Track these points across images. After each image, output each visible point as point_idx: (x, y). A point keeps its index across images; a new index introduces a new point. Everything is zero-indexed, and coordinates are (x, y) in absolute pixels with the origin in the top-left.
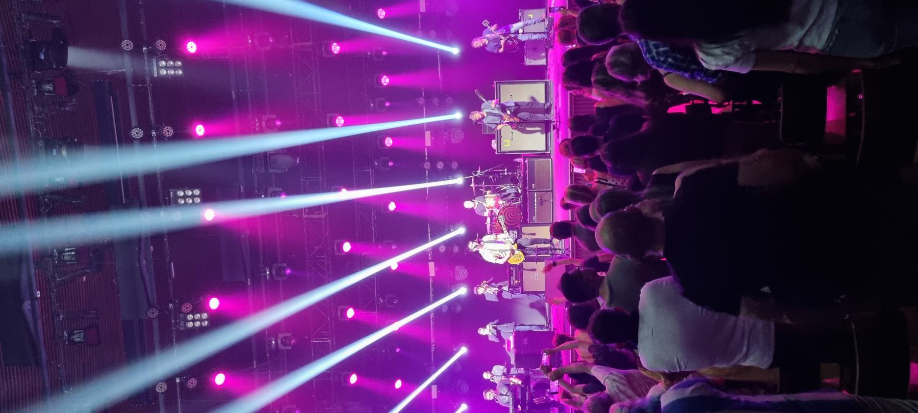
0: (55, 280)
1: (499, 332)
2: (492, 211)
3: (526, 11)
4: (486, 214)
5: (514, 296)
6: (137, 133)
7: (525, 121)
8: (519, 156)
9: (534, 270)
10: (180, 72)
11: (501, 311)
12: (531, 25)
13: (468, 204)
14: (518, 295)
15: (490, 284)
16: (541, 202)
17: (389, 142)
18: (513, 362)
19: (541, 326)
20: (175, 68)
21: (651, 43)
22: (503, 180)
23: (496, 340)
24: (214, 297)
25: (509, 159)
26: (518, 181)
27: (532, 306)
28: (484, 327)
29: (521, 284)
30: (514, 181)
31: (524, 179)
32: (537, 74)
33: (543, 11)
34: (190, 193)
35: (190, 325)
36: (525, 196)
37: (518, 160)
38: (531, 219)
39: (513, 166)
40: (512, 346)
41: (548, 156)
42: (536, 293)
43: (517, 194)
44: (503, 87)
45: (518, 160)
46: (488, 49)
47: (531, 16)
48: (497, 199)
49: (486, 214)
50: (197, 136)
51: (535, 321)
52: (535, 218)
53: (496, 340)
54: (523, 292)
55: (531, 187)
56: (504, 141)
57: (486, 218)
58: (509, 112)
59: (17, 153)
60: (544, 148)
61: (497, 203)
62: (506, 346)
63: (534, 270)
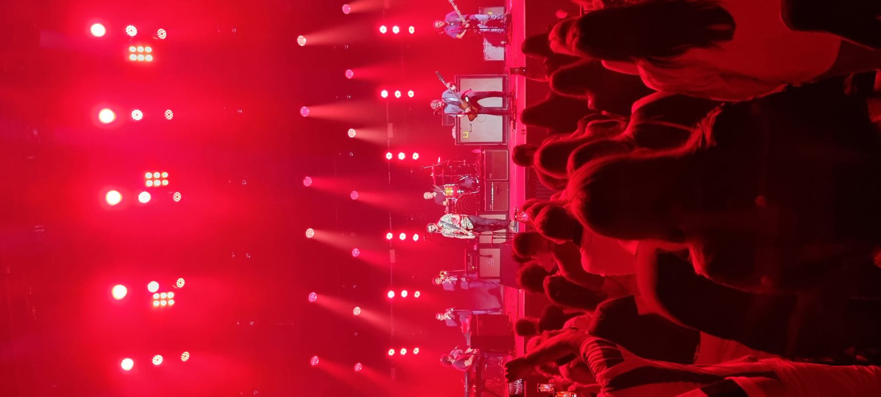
2: (450, 201)
4: (445, 203)
5: (472, 285)
6: (628, 260)
8: (477, 147)
9: (490, 256)
13: (427, 196)
16: (497, 192)
20: (144, 53)
22: (464, 171)
25: (469, 149)
26: (475, 172)
28: (443, 312)
29: (478, 270)
30: (471, 172)
32: (493, 69)
33: (502, 9)
36: (483, 188)
37: (479, 151)
38: (488, 208)
39: (472, 157)
40: (468, 328)
41: (505, 147)
43: (475, 185)
45: (479, 151)
48: (455, 189)
50: (129, 37)
51: (490, 305)
52: (492, 206)
55: (488, 177)
56: (463, 132)
57: (445, 207)
59: (632, 137)
60: (501, 140)
63: (490, 256)
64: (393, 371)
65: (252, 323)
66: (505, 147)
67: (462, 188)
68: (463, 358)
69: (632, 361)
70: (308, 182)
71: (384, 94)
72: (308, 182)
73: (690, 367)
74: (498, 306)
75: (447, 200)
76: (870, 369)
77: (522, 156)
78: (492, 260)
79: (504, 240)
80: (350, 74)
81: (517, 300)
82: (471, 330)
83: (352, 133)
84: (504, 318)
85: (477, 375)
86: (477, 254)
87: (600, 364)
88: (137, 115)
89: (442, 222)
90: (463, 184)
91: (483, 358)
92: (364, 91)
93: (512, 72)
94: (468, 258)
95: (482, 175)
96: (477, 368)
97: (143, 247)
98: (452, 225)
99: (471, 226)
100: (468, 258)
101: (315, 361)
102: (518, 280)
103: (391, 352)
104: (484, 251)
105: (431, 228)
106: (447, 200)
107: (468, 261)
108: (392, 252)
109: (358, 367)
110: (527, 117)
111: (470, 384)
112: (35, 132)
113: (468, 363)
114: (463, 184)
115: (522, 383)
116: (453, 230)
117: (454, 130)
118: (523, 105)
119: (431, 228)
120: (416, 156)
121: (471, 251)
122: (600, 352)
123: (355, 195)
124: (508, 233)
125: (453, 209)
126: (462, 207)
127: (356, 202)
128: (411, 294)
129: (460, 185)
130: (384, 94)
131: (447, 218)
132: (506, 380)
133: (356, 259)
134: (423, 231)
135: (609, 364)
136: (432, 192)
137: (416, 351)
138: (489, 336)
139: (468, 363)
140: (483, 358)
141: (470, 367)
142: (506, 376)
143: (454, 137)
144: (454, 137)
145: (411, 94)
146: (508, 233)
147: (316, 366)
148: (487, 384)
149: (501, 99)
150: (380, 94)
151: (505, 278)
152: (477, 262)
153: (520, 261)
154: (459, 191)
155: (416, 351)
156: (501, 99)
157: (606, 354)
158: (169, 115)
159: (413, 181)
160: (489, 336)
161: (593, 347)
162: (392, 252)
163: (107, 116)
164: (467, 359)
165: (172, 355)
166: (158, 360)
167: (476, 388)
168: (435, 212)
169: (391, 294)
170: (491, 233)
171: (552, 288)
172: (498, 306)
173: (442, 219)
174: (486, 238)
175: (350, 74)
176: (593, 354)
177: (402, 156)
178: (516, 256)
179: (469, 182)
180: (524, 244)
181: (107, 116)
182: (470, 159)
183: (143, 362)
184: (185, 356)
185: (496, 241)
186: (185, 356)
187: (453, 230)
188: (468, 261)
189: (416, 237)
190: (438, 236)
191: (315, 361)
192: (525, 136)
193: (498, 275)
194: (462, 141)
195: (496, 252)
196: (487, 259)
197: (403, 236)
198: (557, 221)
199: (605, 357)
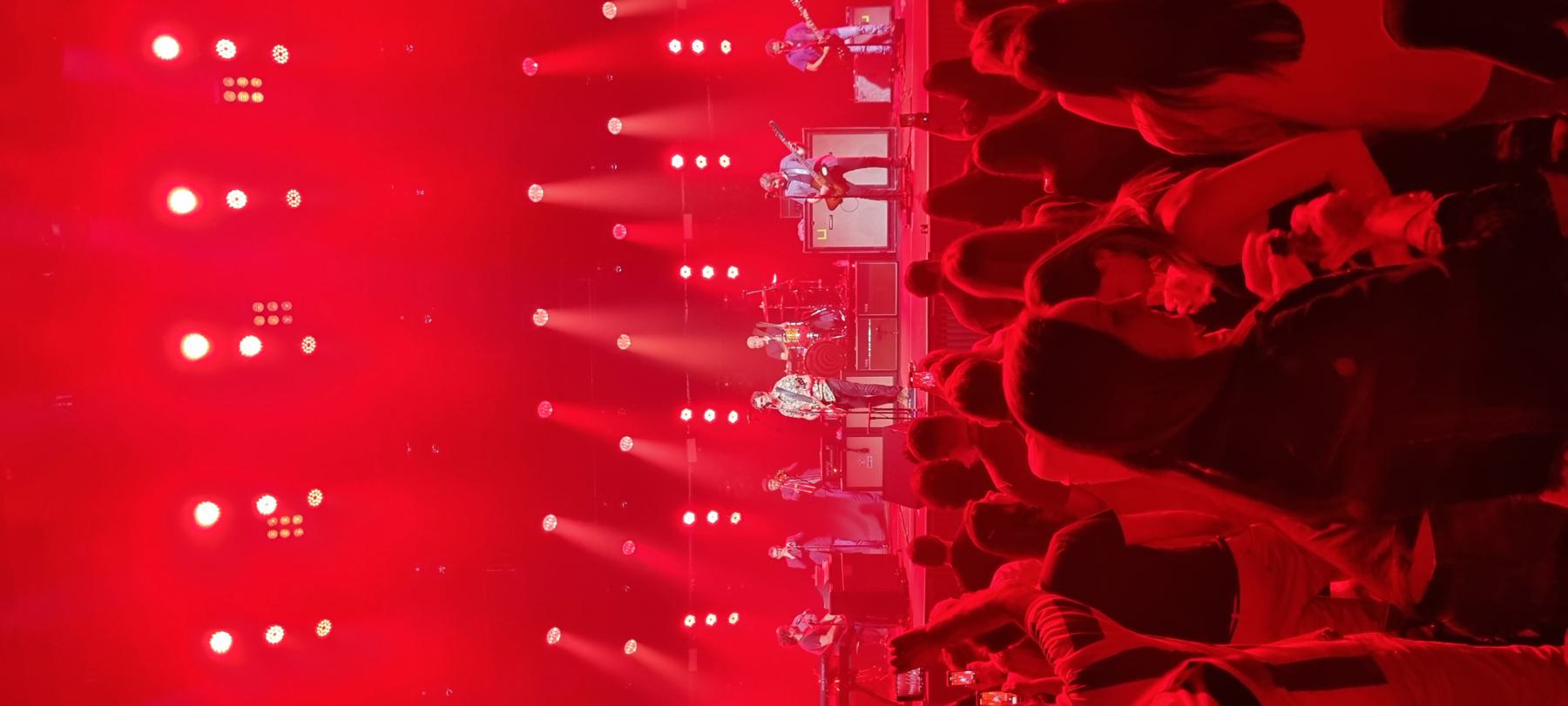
1: (806, 554)
3: (858, 11)
4: (784, 356)
8: (843, 257)
9: (866, 451)
10: (258, 97)
11: (808, 518)
12: (865, 28)
15: (791, 475)
16: (878, 336)
17: (620, 231)
20: (250, 89)
21: (1272, 279)
22: (818, 299)
23: (802, 566)
24: (216, 654)
27: (865, 510)
29: (844, 475)
30: (832, 301)
31: (851, 294)
32: (873, 117)
37: (845, 263)
40: (826, 579)
41: (892, 257)
43: (838, 323)
45: (845, 263)
46: (790, 60)
47: (867, 18)
48: (803, 331)
49: (784, 356)
51: (862, 537)
52: (868, 362)
53: (802, 566)
54: (846, 489)
55: (861, 310)
58: (825, 171)
60: (884, 244)
62: (815, 577)
63: (866, 451)
64: (693, 653)
65: (442, 569)
67: (814, 330)
68: (814, 630)
69: (1118, 638)
77: (923, 279)
78: (869, 457)
79: (891, 422)
80: (615, 126)
82: (830, 581)
83: (620, 231)
85: (842, 663)
86: (842, 447)
89: (779, 389)
90: (817, 323)
94: (826, 453)
97: (237, 430)
98: (796, 397)
104: (855, 442)
105: (759, 402)
109: (631, 647)
111: (829, 677)
112: (56, 230)
113: (825, 640)
116: (798, 404)
117: (801, 226)
119: (759, 402)
120: (733, 272)
123: (624, 343)
124: (898, 410)
125: (798, 366)
129: (811, 323)
131: (787, 383)
132: (892, 669)
134: (745, 406)
135: (1078, 642)
138: (864, 591)
139: (825, 640)
141: (830, 647)
142: (894, 663)
143: (802, 238)
144: (802, 238)
146: (898, 410)
150: (669, 160)
151: (893, 489)
152: (841, 461)
154: (810, 335)
157: (1072, 625)
160: (864, 591)
163: (182, 201)
164: (825, 633)
167: (840, 685)
168: (768, 371)
172: (878, 536)
173: (779, 384)
175: (615, 126)
187: (798, 404)
188: (826, 458)
189: (733, 417)
190: (772, 414)
191: (554, 636)
193: (880, 484)
194: (815, 245)
195: (877, 443)
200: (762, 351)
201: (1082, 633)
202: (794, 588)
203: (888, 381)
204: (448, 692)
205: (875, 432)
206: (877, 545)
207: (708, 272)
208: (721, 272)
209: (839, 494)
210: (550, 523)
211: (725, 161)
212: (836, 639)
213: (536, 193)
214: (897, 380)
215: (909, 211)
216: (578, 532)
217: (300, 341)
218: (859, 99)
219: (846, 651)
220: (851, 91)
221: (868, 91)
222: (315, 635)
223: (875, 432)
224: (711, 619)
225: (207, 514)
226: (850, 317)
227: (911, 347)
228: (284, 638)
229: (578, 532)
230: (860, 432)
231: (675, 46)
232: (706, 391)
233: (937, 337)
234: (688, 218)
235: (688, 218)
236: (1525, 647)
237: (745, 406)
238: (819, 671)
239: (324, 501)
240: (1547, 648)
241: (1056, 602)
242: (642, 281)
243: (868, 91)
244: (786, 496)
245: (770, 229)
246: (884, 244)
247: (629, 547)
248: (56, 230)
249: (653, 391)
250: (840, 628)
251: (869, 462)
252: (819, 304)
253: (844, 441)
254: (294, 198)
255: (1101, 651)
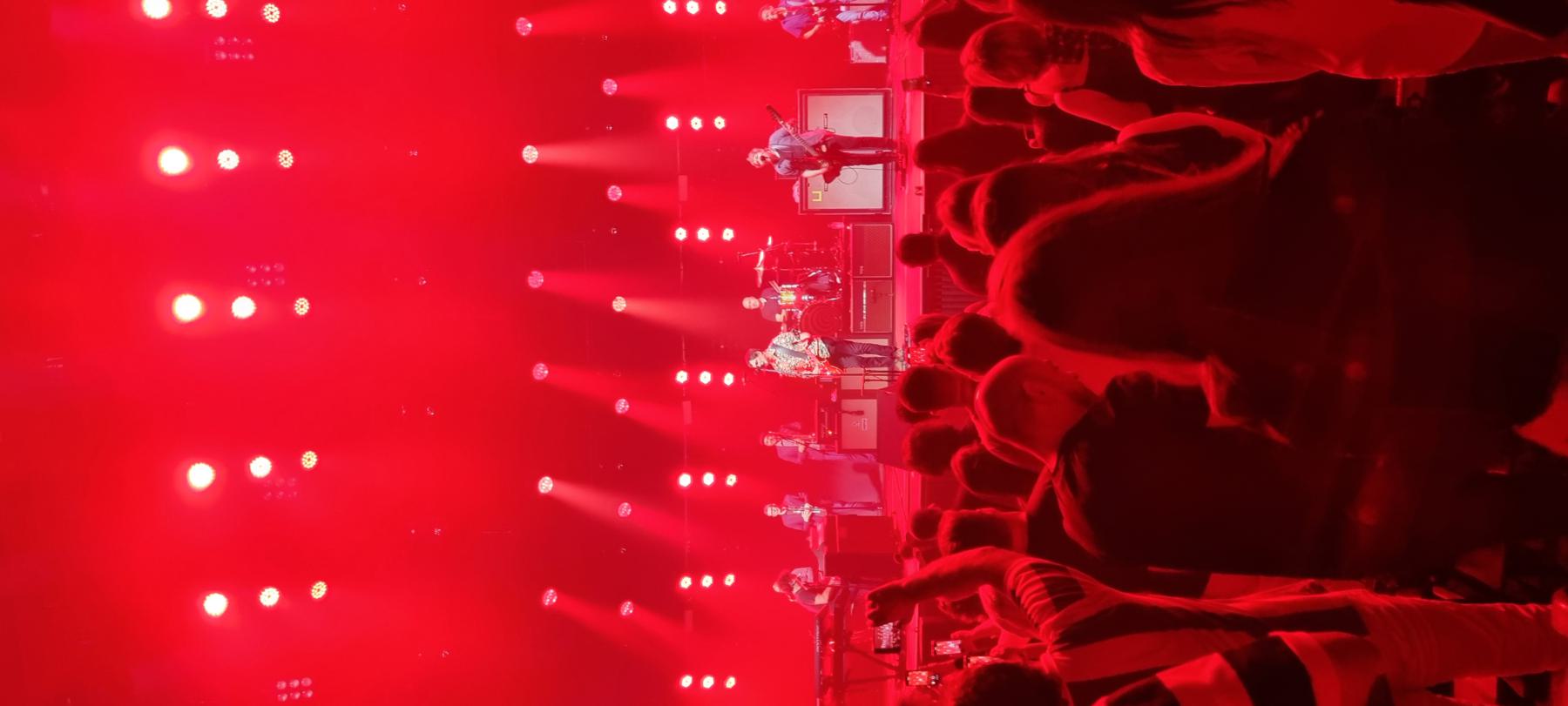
0: (902, 673)
2: (790, 313)
4: (779, 318)
7: (853, 156)
8: (839, 219)
9: (860, 413)
11: (810, 480)
13: (749, 303)
14: (834, 456)
16: (873, 298)
18: (822, 567)
19: (870, 506)
22: (814, 261)
27: (858, 468)
29: (838, 437)
30: (828, 263)
34: (296, 683)
35: (308, 682)
36: (847, 291)
37: (840, 225)
40: (820, 542)
41: (888, 219)
42: (862, 452)
43: (834, 286)
44: (812, 100)
45: (840, 225)
46: (785, 27)
48: (798, 292)
51: (859, 498)
52: (863, 325)
54: (841, 451)
55: (856, 272)
60: (880, 206)
61: (799, 298)
63: (860, 413)
64: (689, 614)
65: (437, 531)
66: (888, 219)
67: (810, 292)
68: (807, 587)
69: (1102, 594)
70: (536, 280)
71: (672, 123)
72: (536, 280)
73: (1205, 604)
74: (873, 498)
75: (784, 312)
76: (1528, 610)
77: (914, 250)
78: (864, 419)
79: (885, 385)
81: (906, 490)
82: (825, 543)
83: (615, 193)
84: (884, 523)
85: (836, 624)
86: (836, 410)
87: (1042, 609)
88: (229, 159)
89: (775, 346)
90: (813, 285)
91: (846, 591)
92: (636, 118)
93: (906, 85)
94: (821, 415)
95: (847, 269)
96: (836, 611)
97: (225, 393)
98: (791, 354)
99: (825, 354)
100: (821, 415)
101: (550, 597)
102: (907, 457)
103: (686, 582)
104: (850, 404)
105: (758, 361)
106: (784, 312)
107: (821, 420)
108: (687, 405)
109: (627, 609)
110: (928, 154)
111: (824, 639)
112: (45, 191)
113: (822, 599)
114: (813, 285)
115: (894, 631)
116: (794, 361)
117: (796, 188)
118: (918, 133)
119: (758, 361)
120: (728, 234)
121: (826, 403)
122: (1042, 585)
124: (892, 372)
125: (791, 323)
126: (814, 323)
127: (622, 316)
128: (720, 479)
129: (806, 285)
130: (672, 123)
131: (783, 339)
132: (870, 621)
133: (623, 417)
134: (741, 368)
135: (1059, 604)
136: (758, 297)
137: (730, 580)
138: (853, 550)
139: (822, 599)
140: (846, 591)
141: (825, 608)
142: (870, 617)
143: (797, 199)
144: (797, 199)
145: (720, 123)
146: (892, 372)
147: (552, 607)
148: (853, 638)
149: (875, 102)
150: (664, 123)
151: (885, 452)
152: (836, 424)
153: (910, 418)
154: (805, 298)
155: (730, 580)
156: (880, 166)
157: (1051, 587)
158: (286, 159)
159: (723, 278)
160: (853, 550)
161: (1027, 578)
162: (687, 405)
163: (173, 161)
164: (821, 592)
165: (294, 589)
166: (270, 597)
167: (835, 646)
168: (763, 332)
169: (685, 480)
170: (861, 370)
171: (968, 462)
172: (873, 498)
173: (775, 341)
174: (854, 378)
176: (1031, 590)
177: (703, 234)
178: (903, 409)
179: (824, 281)
180: (919, 390)
181: (173, 161)
182: (822, 243)
183: (243, 600)
184: (319, 590)
185: (869, 386)
186: (319, 590)
187: (794, 361)
188: (821, 420)
189: (729, 379)
190: (768, 375)
191: (550, 597)
192: (922, 199)
193: (874, 446)
194: (811, 207)
195: (871, 406)
196: (854, 417)
197: (705, 377)
198: (978, 343)
199: (1050, 594)
200: (756, 312)
201: (1062, 593)
202: (793, 544)
203: (884, 342)
204: (445, 653)
205: (869, 394)
206: (870, 506)
207: (707, 581)
208: (716, 234)
209: (834, 456)
210: (546, 485)
211: (720, 123)
212: (831, 598)
213: (530, 154)
214: (892, 341)
215: (904, 171)
216: (575, 495)
217: (293, 302)
218: (854, 60)
219: (840, 613)
220: (847, 53)
221: (860, 53)
222: (311, 597)
223: (869, 394)
224: (709, 479)
225: (201, 476)
226: (845, 278)
227: (902, 315)
228: (280, 600)
229: (575, 495)
230: (855, 394)
231: (681, 234)
232: (701, 353)
233: (932, 297)
234: (683, 180)
235: (683, 180)
236: (1509, 605)
237: (741, 368)
238: (814, 633)
239: (319, 463)
240: (1532, 607)
241: (1033, 566)
242: (641, 249)
243: (860, 53)
244: (823, 379)
245: (766, 200)
246: (880, 206)
247: (625, 509)
248: (45, 191)
249: (652, 350)
250: (835, 589)
251: (864, 423)
252: (814, 266)
253: (838, 404)
254: (286, 159)
255: (1080, 611)
